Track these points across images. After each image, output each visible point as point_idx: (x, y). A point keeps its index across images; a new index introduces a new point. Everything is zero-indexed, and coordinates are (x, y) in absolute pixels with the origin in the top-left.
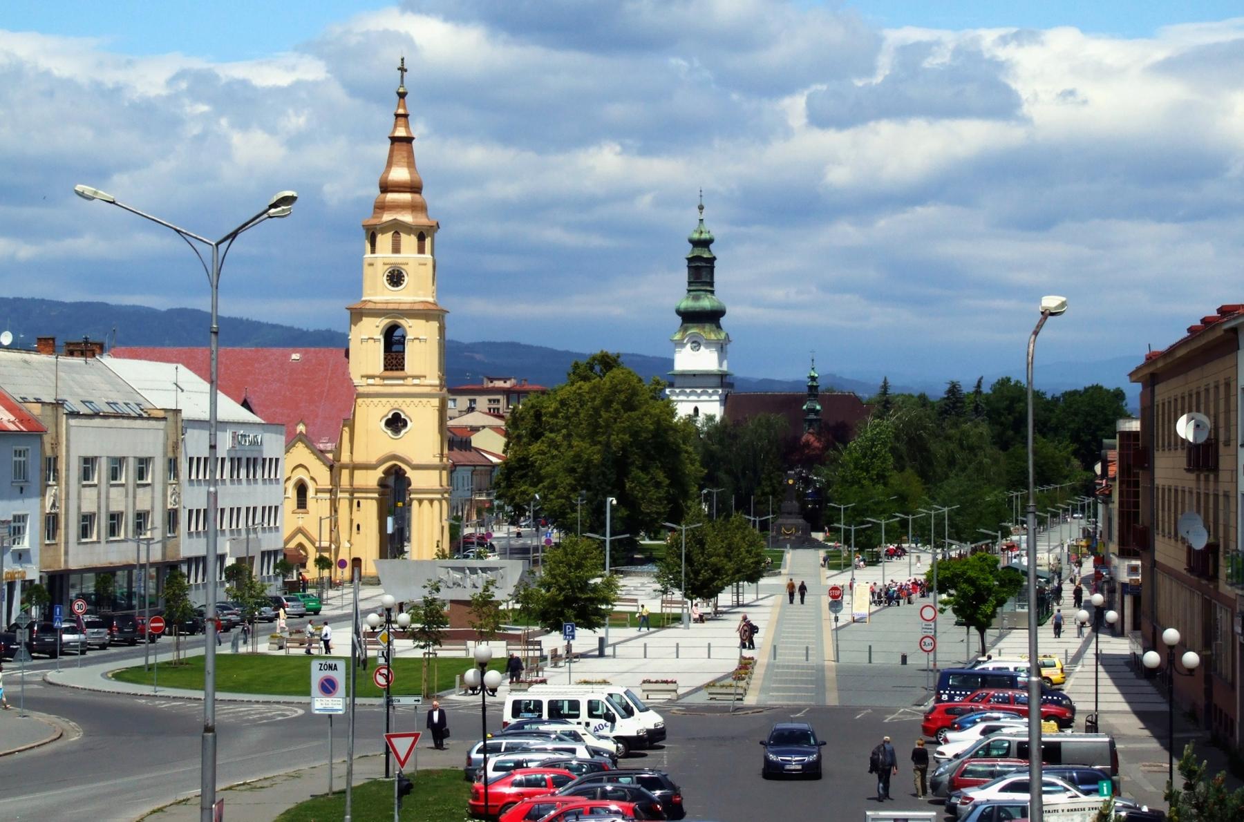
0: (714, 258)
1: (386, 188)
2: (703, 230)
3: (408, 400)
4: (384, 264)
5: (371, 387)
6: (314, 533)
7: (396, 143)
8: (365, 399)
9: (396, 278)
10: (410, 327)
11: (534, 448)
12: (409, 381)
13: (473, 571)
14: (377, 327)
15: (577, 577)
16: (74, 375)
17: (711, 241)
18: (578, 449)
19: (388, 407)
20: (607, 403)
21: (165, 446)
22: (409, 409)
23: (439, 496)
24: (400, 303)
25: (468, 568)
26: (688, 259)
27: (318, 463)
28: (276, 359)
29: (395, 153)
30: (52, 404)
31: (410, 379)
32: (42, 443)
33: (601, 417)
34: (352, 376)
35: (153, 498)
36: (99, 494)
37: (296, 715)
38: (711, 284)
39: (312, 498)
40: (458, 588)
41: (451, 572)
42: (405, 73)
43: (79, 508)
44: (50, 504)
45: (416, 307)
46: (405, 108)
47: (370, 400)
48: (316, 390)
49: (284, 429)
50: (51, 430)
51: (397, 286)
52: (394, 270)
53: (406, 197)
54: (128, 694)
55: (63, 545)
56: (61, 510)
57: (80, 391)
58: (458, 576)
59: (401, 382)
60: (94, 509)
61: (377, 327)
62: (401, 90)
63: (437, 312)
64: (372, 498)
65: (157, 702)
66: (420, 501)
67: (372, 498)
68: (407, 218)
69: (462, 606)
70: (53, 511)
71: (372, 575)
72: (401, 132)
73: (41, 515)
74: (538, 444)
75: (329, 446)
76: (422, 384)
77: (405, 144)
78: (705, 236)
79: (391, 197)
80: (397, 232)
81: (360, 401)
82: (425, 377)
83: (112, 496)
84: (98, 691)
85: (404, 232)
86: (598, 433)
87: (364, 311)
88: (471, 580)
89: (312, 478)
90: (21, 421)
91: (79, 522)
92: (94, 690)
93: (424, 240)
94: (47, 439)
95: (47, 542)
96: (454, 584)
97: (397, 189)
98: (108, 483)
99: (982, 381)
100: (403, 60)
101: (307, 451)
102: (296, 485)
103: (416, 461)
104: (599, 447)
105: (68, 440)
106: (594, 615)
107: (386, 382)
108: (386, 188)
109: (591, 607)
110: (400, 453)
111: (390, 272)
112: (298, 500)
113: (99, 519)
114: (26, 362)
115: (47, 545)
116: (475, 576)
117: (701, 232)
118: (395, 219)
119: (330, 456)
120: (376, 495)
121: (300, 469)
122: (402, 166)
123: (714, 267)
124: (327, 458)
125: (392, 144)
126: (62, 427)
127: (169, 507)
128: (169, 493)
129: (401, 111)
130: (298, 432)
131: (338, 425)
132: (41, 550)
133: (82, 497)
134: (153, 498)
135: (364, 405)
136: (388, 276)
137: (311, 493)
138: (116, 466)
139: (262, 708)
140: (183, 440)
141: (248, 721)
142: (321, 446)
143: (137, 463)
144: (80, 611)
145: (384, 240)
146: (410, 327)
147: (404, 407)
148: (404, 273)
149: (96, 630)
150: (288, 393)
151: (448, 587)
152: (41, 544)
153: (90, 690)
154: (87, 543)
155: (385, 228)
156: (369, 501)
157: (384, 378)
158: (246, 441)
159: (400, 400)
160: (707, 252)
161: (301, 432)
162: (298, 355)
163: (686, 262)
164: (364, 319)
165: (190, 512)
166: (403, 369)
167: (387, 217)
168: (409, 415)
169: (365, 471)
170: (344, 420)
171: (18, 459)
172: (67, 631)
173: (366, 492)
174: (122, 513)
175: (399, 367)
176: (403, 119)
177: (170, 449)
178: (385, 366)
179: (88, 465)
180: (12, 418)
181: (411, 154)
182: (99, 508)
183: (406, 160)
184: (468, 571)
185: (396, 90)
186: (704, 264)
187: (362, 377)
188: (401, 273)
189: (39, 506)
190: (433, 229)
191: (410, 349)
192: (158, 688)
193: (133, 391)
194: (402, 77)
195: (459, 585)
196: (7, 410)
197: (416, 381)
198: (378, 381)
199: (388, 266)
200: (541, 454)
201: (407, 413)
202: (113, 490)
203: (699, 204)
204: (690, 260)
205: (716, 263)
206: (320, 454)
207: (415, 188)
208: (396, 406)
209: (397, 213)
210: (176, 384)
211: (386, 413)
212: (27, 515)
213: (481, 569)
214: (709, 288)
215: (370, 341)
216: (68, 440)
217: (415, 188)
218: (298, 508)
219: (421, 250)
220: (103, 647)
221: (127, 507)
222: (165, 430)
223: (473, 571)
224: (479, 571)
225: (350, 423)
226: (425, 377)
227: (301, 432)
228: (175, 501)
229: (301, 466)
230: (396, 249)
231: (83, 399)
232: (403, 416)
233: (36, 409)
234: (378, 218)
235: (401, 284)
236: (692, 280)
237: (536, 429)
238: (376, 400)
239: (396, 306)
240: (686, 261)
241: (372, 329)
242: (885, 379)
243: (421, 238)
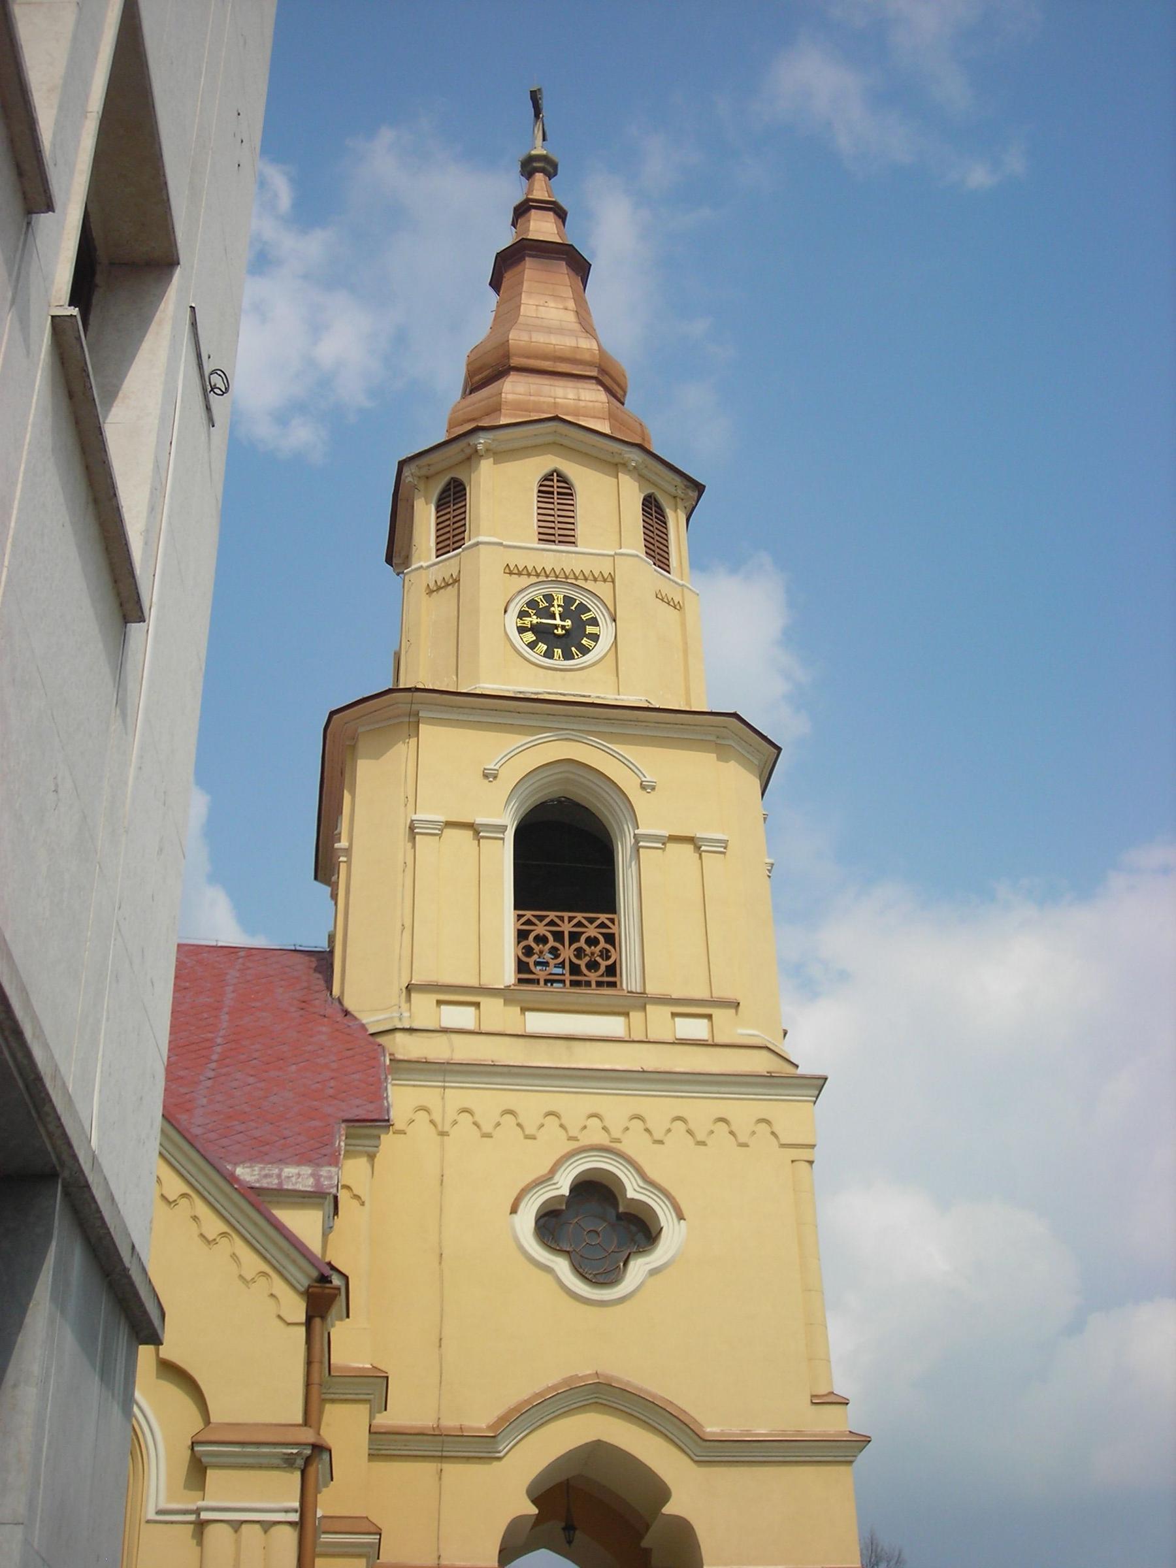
4: (509, 571)
14: (489, 775)
19: (553, 1143)
31: (658, 1015)
61: (489, 775)
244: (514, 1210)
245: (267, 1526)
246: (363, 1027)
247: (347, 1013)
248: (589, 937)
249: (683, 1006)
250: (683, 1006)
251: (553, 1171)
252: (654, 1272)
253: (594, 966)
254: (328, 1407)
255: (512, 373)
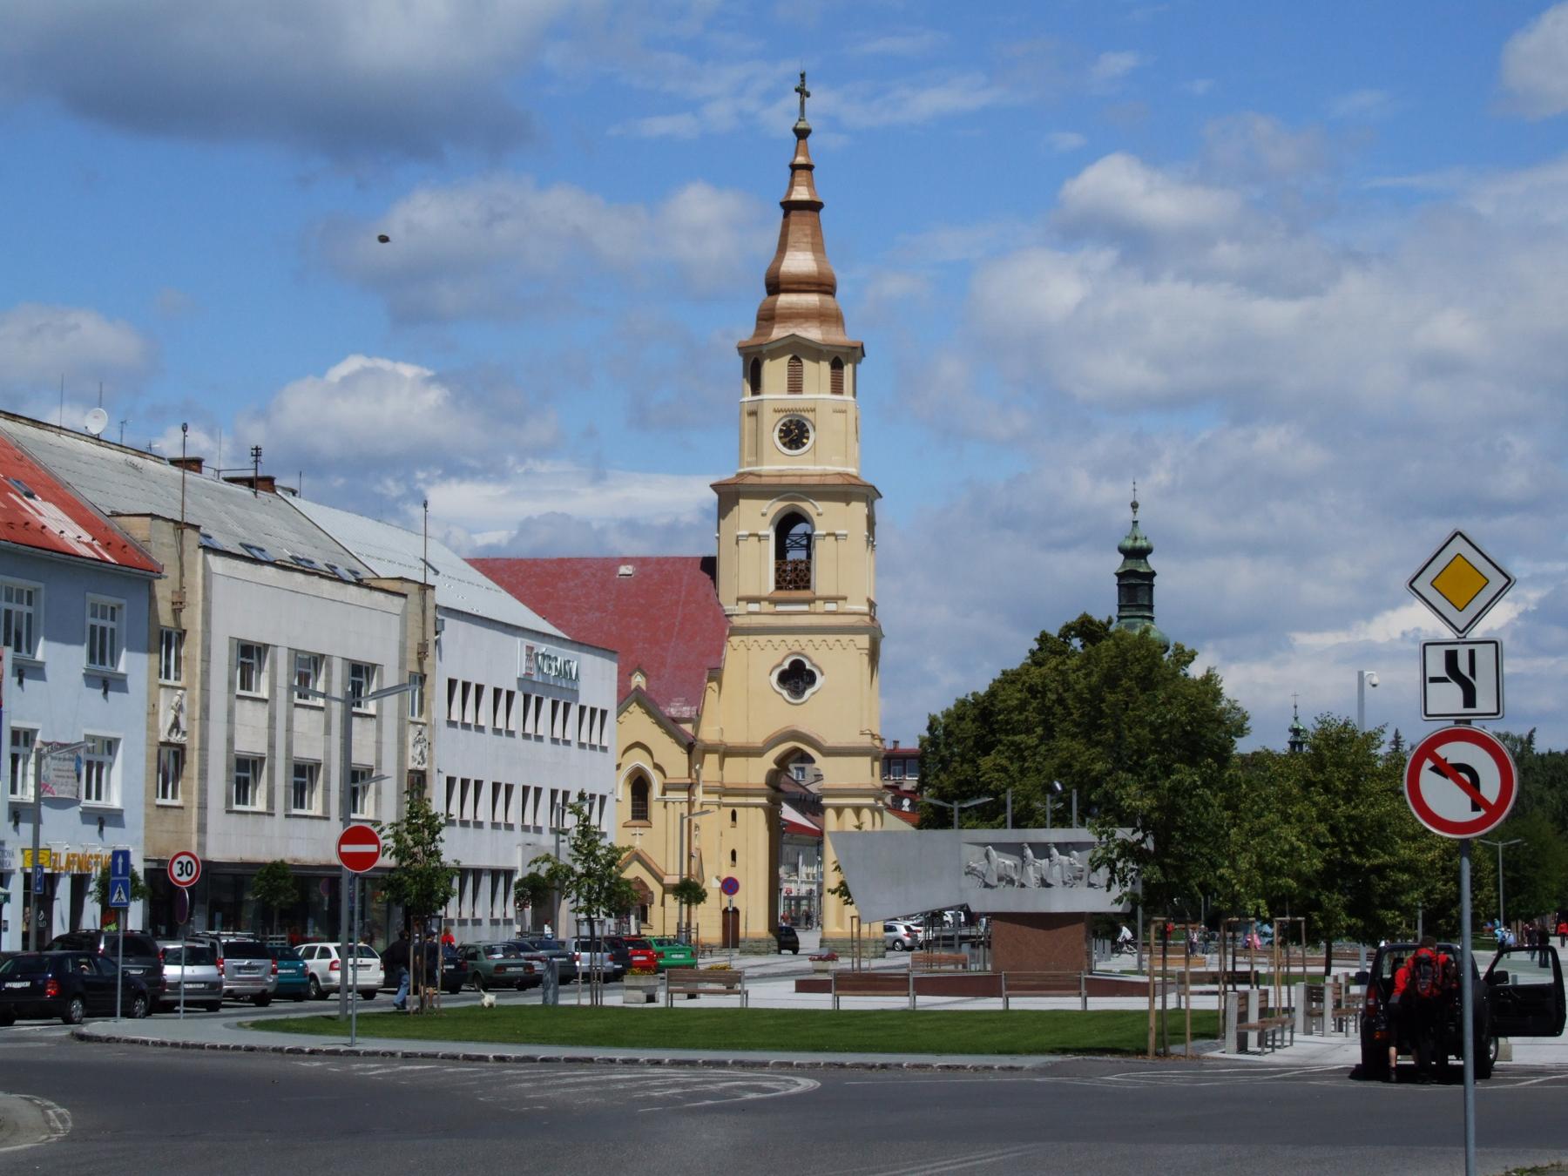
0: (1153, 574)
1: (775, 285)
2: (1138, 536)
3: (817, 638)
4: (776, 411)
5: (753, 617)
6: (658, 861)
7: (793, 212)
8: (744, 638)
9: (794, 434)
10: (819, 515)
11: (986, 763)
12: (820, 606)
13: (1042, 850)
14: (764, 515)
15: (1350, 818)
16: (232, 507)
17: (1148, 551)
18: (1065, 754)
19: (783, 651)
20: (1111, 680)
21: (403, 648)
22: (817, 652)
23: (871, 801)
24: (801, 476)
25: (1031, 845)
26: (1117, 574)
27: (667, 739)
28: (594, 575)
29: (792, 228)
30: (176, 522)
31: (819, 603)
32: (152, 598)
33: (1103, 700)
34: (722, 600)
35: (379, 743)
36: (272, 718)
37: (794, 1090)
38: (1150, 608)
39: (658, 800)
40: (1009, 888)
41: (994, 853)
42: (807, 100)
43: (230, 741)
44: (169, 726)
45: (830, 481)
46: (807, 155)
47: (752, 638)
48: (661, 623)
49: (616, 656)
50: (171, 572)
51: (798, 448)
52: (791, 421)
53: (812, 300)
54: (275, 1050)
55: (195, 811)
56: (192, 738)
57: (240, 531)
58: (1009, 861)
59: (805, 608)
60: (260, 748)
61: (764, 515)
62: (801, 126)
63: (865, 491)
64: (756, 806)
65: (355, 1066)
66: (839, 810)
67: (756, 806)
68: (812, 333)
69: (1026, 929)
70: (175, 738)
71: (757, 937)
72: (801, 194)
73: (148, 745)
74: (992, 757)
75: (687, 711)
76: (841, 610)
77: (808, 213)
78: (1141, 543)
79: (784, 300)
80: (796, 359)
81: (735, 640)
82: (845, 599)
83: (297, 727)
84: (194, 1046)
85: (809, 358)
86: (1100, 727)
87: (741, 489)
88: (1036, 870)
89: (657, 767)
90: (107, 546)
91: (229, 770)
92: (186, 1046)
93: (842, 368)
94: (164, 591)
95: (160, 801)
96: (1000, 879)
97: (795, 287)
98: (290, 699)
99: (1535, 735)
100: (803, 76)
101: (647, 720)
102: (630, 776)
103: (830, 741)
104: (1099, 749)
105: (207, 599)
106: (1388, 908)
107: (780, 608)
108: (775, 285)
109: (1382, 886)
110: (804, 728)
111: (784, 425)
112: (633, 805)
113: (271, 769)
114: (134, 467)
115: (158, 806)
116: (1045, 862)
117: (1136, 539)
118: (793, 335)
119: (688, 727)
120: (763, 800)
121: (637, 751)
122: (805, 250)
123: (1153, 585)
124: (683, 732)
125: (786, 215)
126: (195, 572)
127: (412, 765)
128: (410, 740)
129: (800, 160)
130: (633, 687)
131: (701, 676)
132: (147, 815)
133: (237, 721)
134: (379, 743)
135: (742, 649)
136: (781, 431)
137: (655, 792)
138: (308, 666)
139: (682, 1075)
140: (437, 642)
141: (650, 1101)
142: (673, 711)
143: (348, 671)
144: (185, 878)
145: (775, 371)
146: (819, 515)
147: (809, 651)
148: (809, 426)
149: (246, 962)
150: (614, 628)
151: (987, 886)
152: (148, 805)
153: (175, 1045)
154: (246, 813)
155: (775, 352)
156: (752, 810)
157: (775, 602)
158: (550, 668)
159: (803, 639)
160: (1144, 565)
161: (638, 686)
162: (630, 567)
163: (1116, 579)
164: (742, 502)
165: (450, 781)
166: (807, 586)
167: (779, 332)
168: (818, 663)
169: (743, 759)
170: (711, 669)
171: (99, 622)
172: (175, 958)
173: (746, 795)
174: (318, 765)
175: (802, 584)
176: (804, 173)
177: (412, 656)
178: (777, 582)
179: (250, 655)
180: (87, 538)
181: (817, 231)
182: (272, 746)
183: (810, 240)
184: (1029, 852)
185: (793, 125)
186: (1139, 581)
187: (739, 599)
188: (804, 425)
189: (144, 725)
190: (855, 353)
191: (823, 552)
192: (358, 1040)
193: (342, 551)
194: (802, 103)
195: (1011, 882)
196: (77, 523)
197: (831, 607)
198: (766, 606)
199: (782, 415)
200: (998, 771)
201: (815, 661)
202: (298, 712)
203: (1132, 501)
204: (1120, 576)
205: (1156, 580)
206: (670, 726)
207: (824, 285)
208: (797, 648)
209: (796, 326)
210: (424, 561)
211: (778, 661)
212: (117, 740)
213: (1057, 845)
214: (1147, 614)
215: (751, 538)
216: (207, 599)
217: (824, 285)
218: (634, 818)
219: (837, 388)
220: (261, 999)
221: (328, 753)
222: (404, 618)
223: (1042, 850)
224: (1054, 851)
225: (716, 674)
226: (845, 599)
227: (638, 686)
228: (421, 753)
229: (638, 745)
230: (795, 386)
231: (246, 542)
232: (808, 666)
233: (139, 530)
234: (763, 335)
235: (804, 444)
236: (1124, 603)
237: (984, 736)
238: (762, 639)
239: (796, 480)
240: (1116, 578)
241: (758, 517)
242: (1397, 730)
243: (837, 365)
244: (770, 674)
245: (681, 802)
246: (724, 611)
247: (719, 604)
248: (453, 925)
249: (827, 600)
250: (827, 600)
251: (783, 661)
252: (813, 694)
253: (802, 580)
254: (707, 756)
255: (761, 745)
